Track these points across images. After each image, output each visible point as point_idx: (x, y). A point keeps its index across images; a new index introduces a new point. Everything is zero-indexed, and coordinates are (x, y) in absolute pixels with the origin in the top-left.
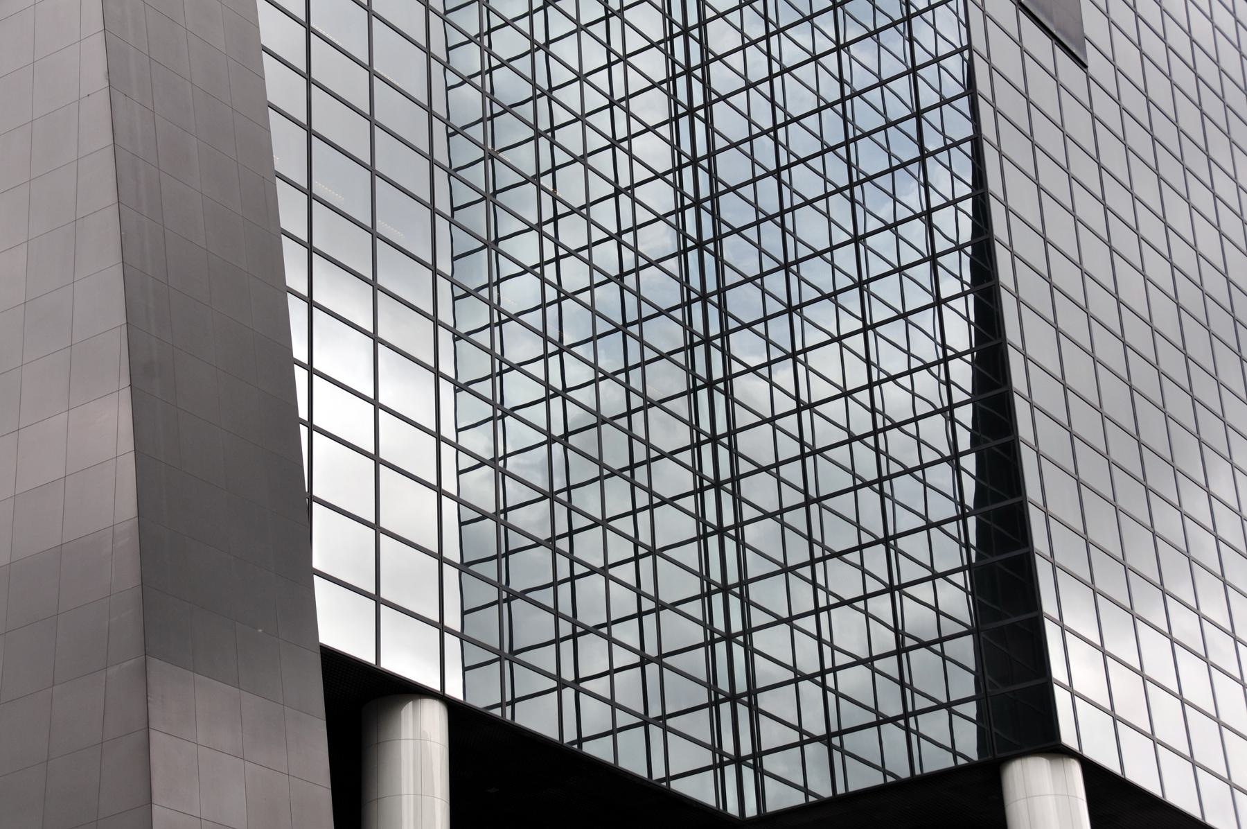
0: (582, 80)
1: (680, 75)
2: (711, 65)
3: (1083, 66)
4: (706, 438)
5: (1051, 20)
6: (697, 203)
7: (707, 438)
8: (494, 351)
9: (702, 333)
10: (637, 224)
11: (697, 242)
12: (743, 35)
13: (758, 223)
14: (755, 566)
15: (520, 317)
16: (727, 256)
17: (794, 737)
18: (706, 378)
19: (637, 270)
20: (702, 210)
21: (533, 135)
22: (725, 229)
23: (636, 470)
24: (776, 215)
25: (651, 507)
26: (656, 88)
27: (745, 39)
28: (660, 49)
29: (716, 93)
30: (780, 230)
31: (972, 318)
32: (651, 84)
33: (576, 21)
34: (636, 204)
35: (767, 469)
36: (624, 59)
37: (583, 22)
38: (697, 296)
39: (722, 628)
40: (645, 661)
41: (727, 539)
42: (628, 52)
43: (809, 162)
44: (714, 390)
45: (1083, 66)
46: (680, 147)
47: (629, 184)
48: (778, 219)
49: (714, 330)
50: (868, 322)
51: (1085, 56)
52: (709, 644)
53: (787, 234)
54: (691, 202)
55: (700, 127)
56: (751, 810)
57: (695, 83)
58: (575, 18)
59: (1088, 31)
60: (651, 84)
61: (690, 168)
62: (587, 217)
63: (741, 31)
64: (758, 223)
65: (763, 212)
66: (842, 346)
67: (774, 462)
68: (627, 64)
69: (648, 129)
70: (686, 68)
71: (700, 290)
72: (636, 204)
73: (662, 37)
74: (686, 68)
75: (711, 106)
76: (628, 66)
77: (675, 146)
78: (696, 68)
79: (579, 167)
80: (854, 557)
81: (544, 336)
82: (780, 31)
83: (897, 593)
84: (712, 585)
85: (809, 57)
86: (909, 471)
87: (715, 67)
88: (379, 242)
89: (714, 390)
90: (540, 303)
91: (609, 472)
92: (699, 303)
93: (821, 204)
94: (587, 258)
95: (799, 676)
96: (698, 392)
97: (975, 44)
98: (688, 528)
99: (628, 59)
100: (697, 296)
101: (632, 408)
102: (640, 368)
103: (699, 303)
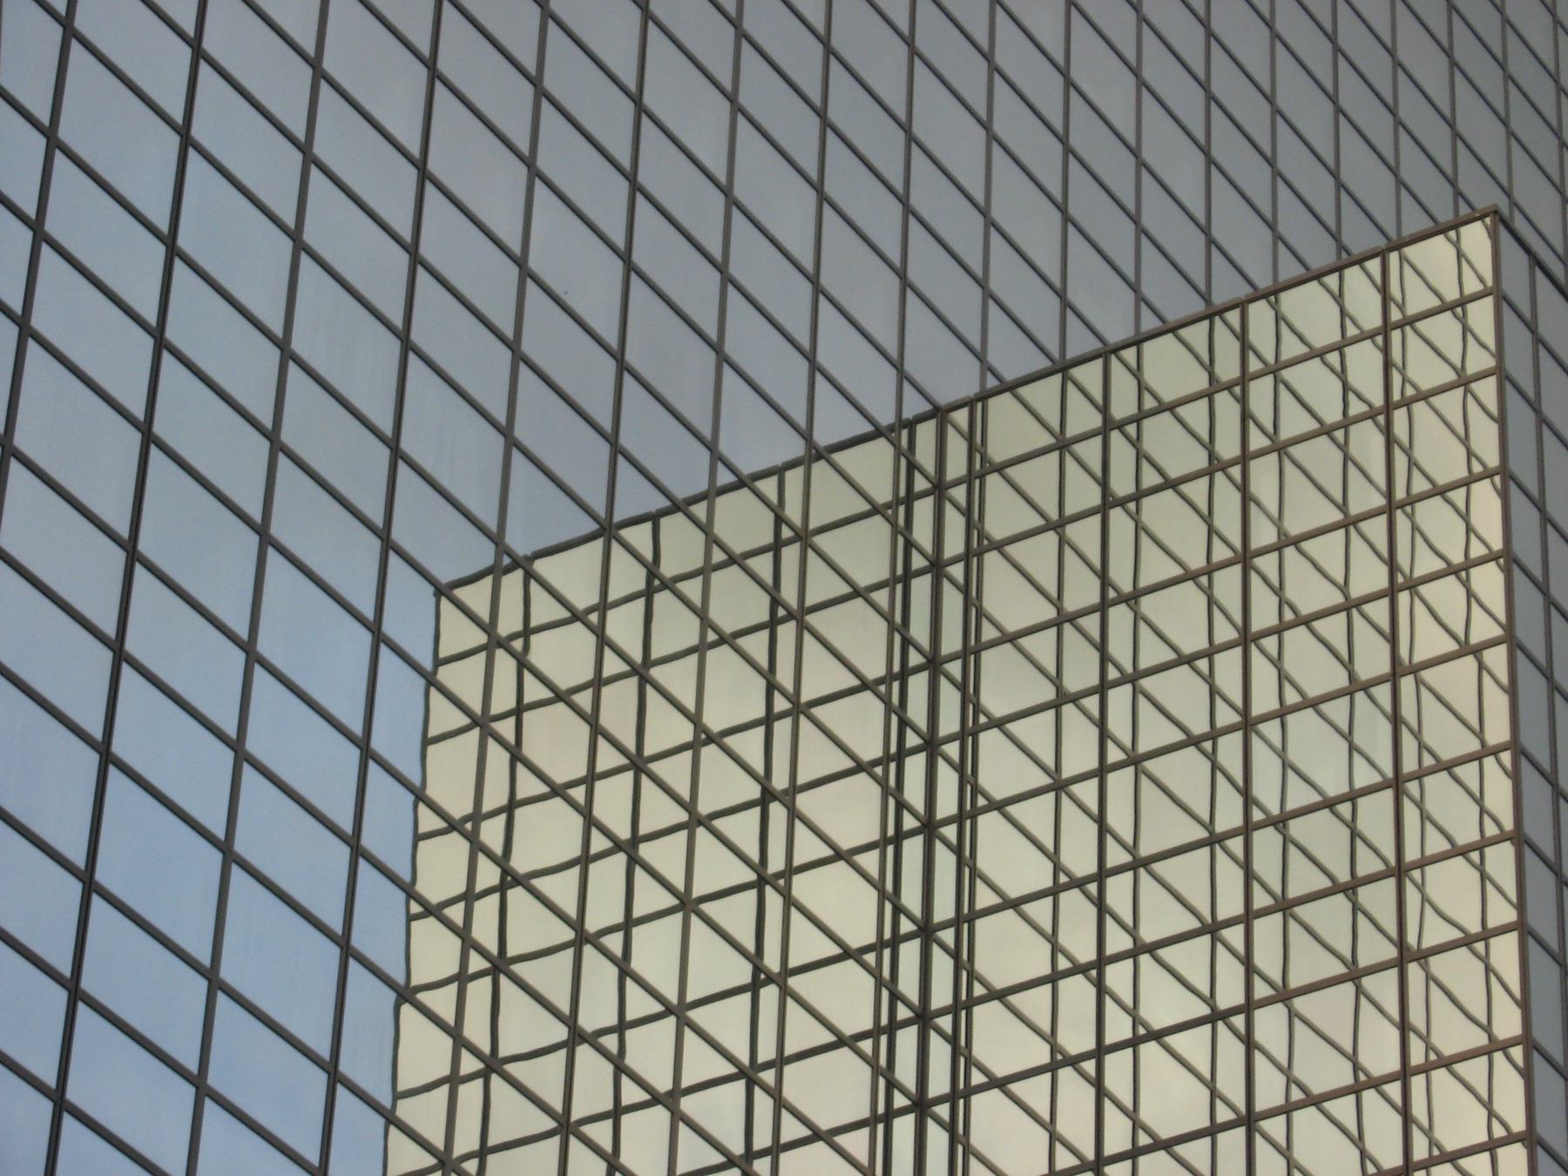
1: (921, 572)
2: (986, 656)
6: (924, 1018)
8: (470, 932)
13: (1054, 892)
22: (985, 898)
24: (1089, 879)
28: (860, 1054)
29: (983, 1070)
30: (1094, 827)
33: (690, 806)
37: (704, 808)
43: (1181, 1149)
48: (1093, 888)
53: (1108, 917)
57: (946, 689)
62: (706, 623)
64: (1054, 892)
69: (816, 1135)
73: (868, 1024)
77: (889, 896)
78: (952, 658)
79: (660, 1114)
82: (1138, 864)
86: (1315, 1101)
87: (987, 1016)
88: (235, 870)
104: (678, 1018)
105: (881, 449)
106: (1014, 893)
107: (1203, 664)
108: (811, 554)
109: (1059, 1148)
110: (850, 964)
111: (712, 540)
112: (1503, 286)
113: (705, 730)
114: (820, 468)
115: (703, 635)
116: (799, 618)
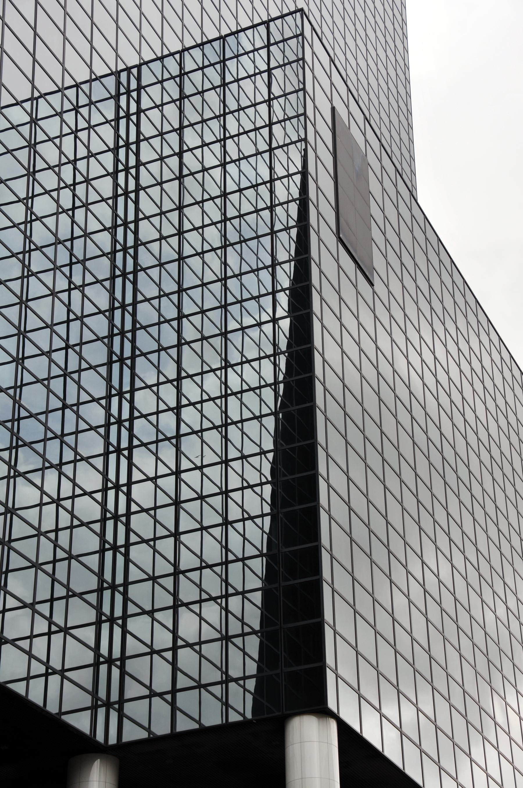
0: (54, 295)
3: (372, 284)
4: (110, 516)
5: (356, 252)
6: (119, 422)
7: (110, 547)
9: (112, 542)
10: (87, 258)
11: (120, 357)
12: (160, 289)
14: (134, 574)
15: (6, 283)
16: (135, 460)
17: (147, 692)
18: (112, 543)
19: (73, 497)
20: (123, 399)
21: (29, 120)
23: (74, 241)
25: (71, 527)
26: (100, 341)
27: (161, 292)
31: (292, 278)
32: (102, 254)
34: (76, 487)
35: (147, 542)
36: (81, 318)
38: (112, 485)
39: (110, 580)
40: (65, 406)
41: (115, 626)
42: (89, 202)
44: (117, 553)
45: (372, 284)
46: (113, 321)
47: (81, 284)
49: (124, 444)
50: (223, 310)
51: (373, 279)
52: (96, 665)
54: (115, 421)
55: (127, 372)
56: (113, 740)
58: (58, 172)
59: (375, 265)
60: (102, 254)
61: (122, 227)
63: (159, 286)
65: (163, 292)
66: (201, 523)
67: (156, 411)
68: (87, 209)
70: (121, 331)
71: (118, 389)
72: (76, 487)
74: (121, 331)
75: (140, 142)
76: (84, 325)
80: (195, 607)
81: (19, 330)
83: (224, 490)
84: (101, 658)
85: (199, 310)
89: (117, 553)
90: (21, 276)
91: (49, 465)
92: (112, 521)
93: (198, 379)
94: (44, 422)
95: (152, 693)
96: (106, 552)
97: (309, 138)
98: (94, 544)
99: (89, 206)
100: (115, 421)
101: (77, 158)
102: (69, 530)
103: (112, 521)
104: (51, 329)
105: (113, 78)
106: (148, 297)
107: (200, 231)
108: (89, 186)
109: (161, 375)
110: (101, 315)
111: (58, 175)
112: (227, 286)
113: (59, 239)
114: (92, 159)
115: (58, 209)
116: (86, 206)
